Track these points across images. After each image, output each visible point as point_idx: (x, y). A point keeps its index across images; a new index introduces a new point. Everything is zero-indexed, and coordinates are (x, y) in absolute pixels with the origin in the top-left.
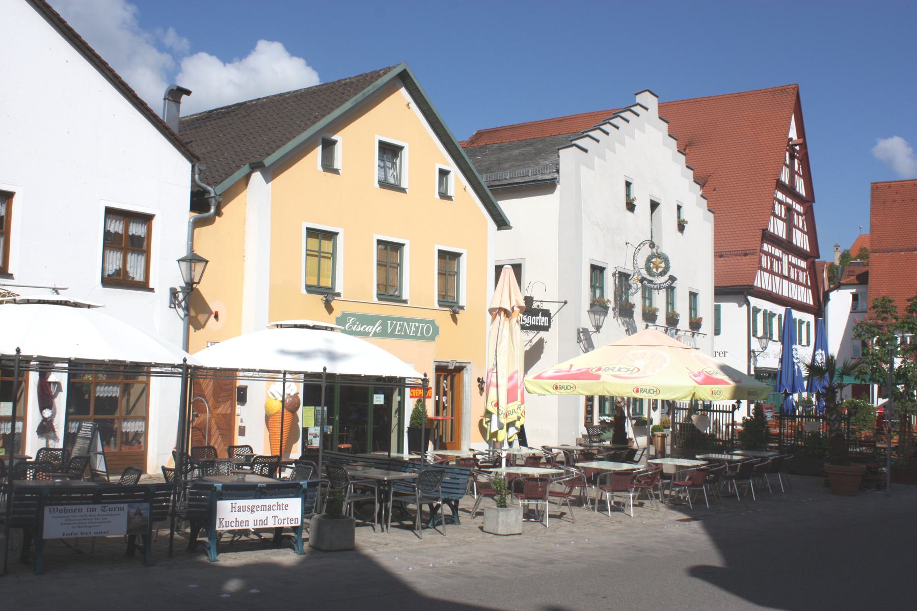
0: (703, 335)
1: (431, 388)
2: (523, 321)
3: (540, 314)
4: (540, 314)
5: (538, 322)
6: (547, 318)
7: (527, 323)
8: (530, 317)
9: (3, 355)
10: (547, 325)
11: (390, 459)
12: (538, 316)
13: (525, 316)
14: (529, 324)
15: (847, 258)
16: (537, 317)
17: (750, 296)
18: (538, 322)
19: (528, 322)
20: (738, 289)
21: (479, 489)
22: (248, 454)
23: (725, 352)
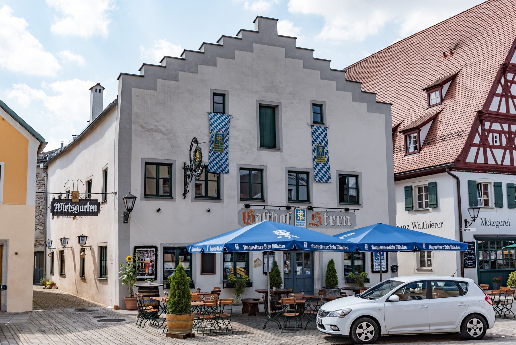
0: (279, 207)
1: (113, 260)
2: (71, 209)
3: (88, 204)
4: (88, 204)
5: (87, 209)
6: (96, 206)
7: (75, 211)
8: (78, 206)
9: (514, 208)
10: (96, 211)
11: (508, 114)
12: (87, 205)
13: (73, 206)
14: (77, 211)
15: (242, 291)
16: (85, 206)
17: (496, 91)
18: (87, 209)
19: (76, 210)
20: (394, 331)
21: (409, 285)
22: (183, 259)
23: (441, 223)
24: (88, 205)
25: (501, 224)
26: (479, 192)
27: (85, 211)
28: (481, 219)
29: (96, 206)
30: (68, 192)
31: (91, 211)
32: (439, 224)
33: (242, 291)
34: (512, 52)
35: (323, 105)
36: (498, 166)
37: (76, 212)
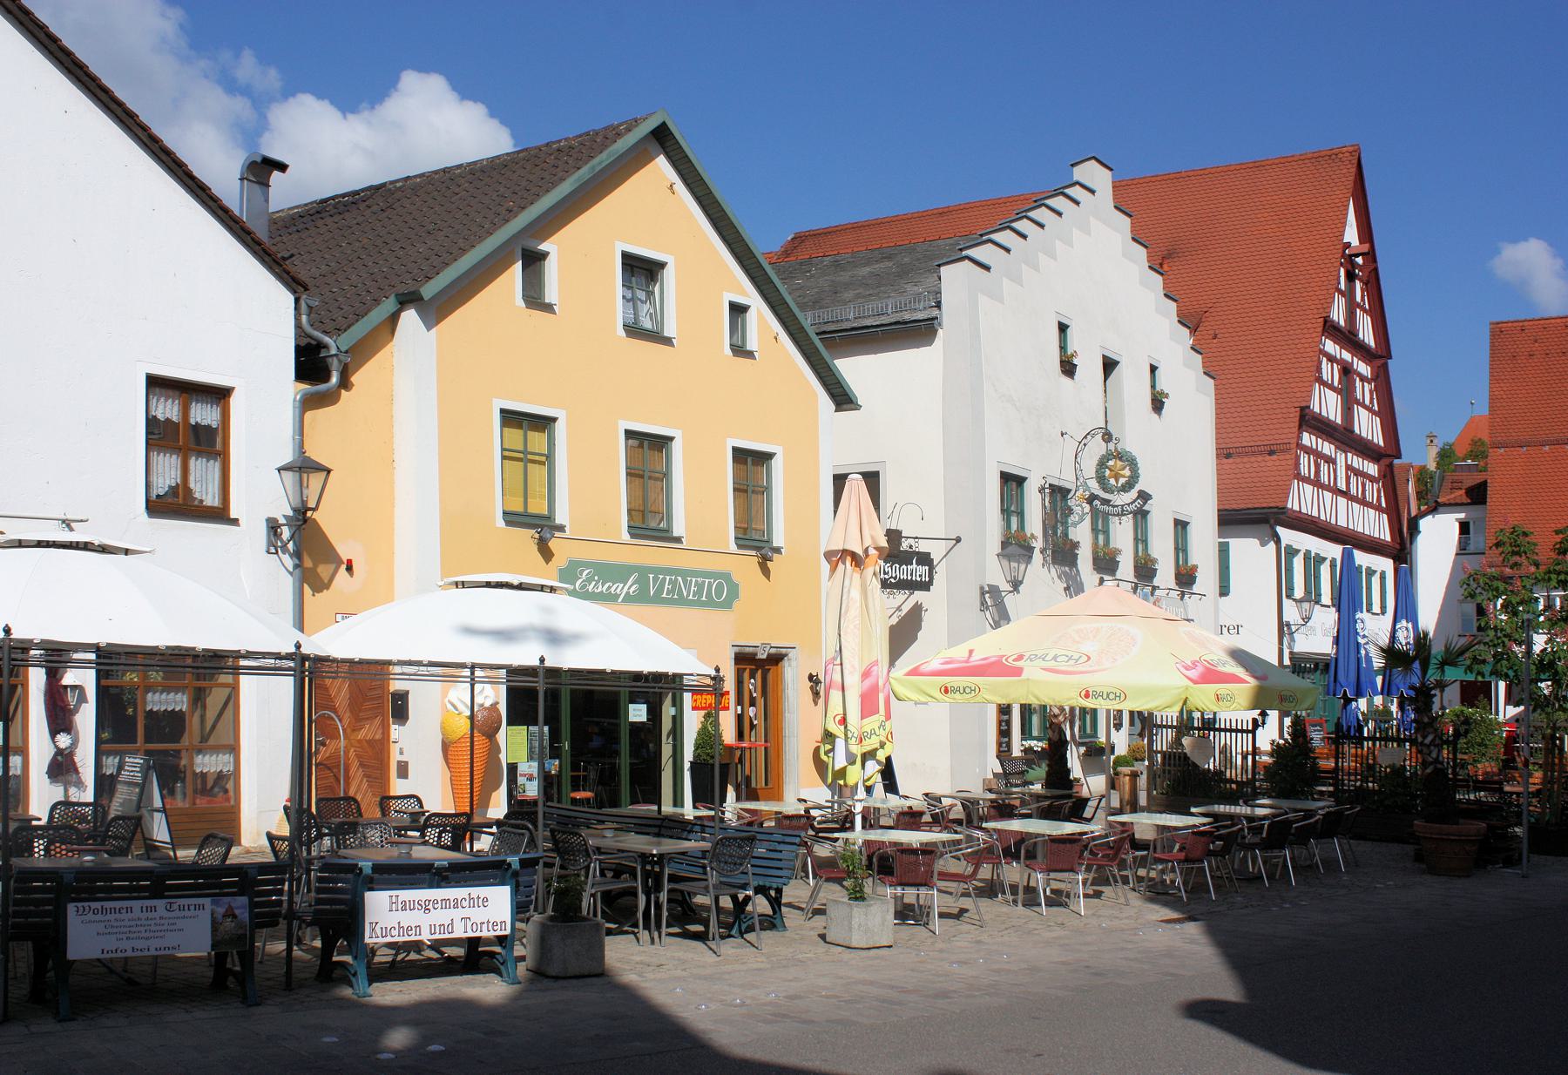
2: (885, 573)
4: (914, 561)
6: (927, 568)
7: (891, 577)
8: (898, 566)
13: (888, 565)
16: (909, 566)
19: (894, 576)
23: (1238, 626)
24: (914, 565)
25: (1539, 752)
26: (686, 864)
27: (909, 578)
28: (1092, 192)
29: (927, 568)
30: (1480, 439)
31: (919, 579)
32: (1231, 627)
33: (235, 95)
34: (747, 834)
35: (749, 307)
36: (731, 833)
37: (893, 581)
